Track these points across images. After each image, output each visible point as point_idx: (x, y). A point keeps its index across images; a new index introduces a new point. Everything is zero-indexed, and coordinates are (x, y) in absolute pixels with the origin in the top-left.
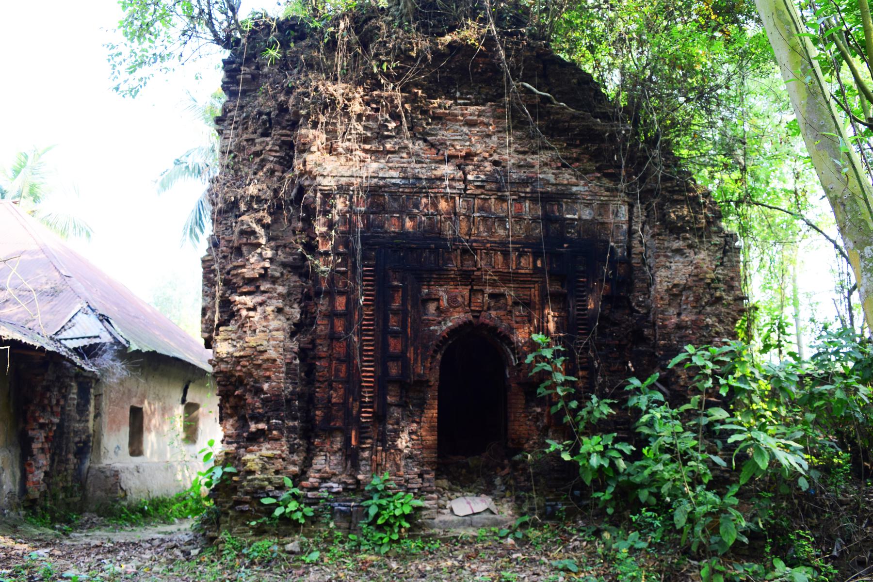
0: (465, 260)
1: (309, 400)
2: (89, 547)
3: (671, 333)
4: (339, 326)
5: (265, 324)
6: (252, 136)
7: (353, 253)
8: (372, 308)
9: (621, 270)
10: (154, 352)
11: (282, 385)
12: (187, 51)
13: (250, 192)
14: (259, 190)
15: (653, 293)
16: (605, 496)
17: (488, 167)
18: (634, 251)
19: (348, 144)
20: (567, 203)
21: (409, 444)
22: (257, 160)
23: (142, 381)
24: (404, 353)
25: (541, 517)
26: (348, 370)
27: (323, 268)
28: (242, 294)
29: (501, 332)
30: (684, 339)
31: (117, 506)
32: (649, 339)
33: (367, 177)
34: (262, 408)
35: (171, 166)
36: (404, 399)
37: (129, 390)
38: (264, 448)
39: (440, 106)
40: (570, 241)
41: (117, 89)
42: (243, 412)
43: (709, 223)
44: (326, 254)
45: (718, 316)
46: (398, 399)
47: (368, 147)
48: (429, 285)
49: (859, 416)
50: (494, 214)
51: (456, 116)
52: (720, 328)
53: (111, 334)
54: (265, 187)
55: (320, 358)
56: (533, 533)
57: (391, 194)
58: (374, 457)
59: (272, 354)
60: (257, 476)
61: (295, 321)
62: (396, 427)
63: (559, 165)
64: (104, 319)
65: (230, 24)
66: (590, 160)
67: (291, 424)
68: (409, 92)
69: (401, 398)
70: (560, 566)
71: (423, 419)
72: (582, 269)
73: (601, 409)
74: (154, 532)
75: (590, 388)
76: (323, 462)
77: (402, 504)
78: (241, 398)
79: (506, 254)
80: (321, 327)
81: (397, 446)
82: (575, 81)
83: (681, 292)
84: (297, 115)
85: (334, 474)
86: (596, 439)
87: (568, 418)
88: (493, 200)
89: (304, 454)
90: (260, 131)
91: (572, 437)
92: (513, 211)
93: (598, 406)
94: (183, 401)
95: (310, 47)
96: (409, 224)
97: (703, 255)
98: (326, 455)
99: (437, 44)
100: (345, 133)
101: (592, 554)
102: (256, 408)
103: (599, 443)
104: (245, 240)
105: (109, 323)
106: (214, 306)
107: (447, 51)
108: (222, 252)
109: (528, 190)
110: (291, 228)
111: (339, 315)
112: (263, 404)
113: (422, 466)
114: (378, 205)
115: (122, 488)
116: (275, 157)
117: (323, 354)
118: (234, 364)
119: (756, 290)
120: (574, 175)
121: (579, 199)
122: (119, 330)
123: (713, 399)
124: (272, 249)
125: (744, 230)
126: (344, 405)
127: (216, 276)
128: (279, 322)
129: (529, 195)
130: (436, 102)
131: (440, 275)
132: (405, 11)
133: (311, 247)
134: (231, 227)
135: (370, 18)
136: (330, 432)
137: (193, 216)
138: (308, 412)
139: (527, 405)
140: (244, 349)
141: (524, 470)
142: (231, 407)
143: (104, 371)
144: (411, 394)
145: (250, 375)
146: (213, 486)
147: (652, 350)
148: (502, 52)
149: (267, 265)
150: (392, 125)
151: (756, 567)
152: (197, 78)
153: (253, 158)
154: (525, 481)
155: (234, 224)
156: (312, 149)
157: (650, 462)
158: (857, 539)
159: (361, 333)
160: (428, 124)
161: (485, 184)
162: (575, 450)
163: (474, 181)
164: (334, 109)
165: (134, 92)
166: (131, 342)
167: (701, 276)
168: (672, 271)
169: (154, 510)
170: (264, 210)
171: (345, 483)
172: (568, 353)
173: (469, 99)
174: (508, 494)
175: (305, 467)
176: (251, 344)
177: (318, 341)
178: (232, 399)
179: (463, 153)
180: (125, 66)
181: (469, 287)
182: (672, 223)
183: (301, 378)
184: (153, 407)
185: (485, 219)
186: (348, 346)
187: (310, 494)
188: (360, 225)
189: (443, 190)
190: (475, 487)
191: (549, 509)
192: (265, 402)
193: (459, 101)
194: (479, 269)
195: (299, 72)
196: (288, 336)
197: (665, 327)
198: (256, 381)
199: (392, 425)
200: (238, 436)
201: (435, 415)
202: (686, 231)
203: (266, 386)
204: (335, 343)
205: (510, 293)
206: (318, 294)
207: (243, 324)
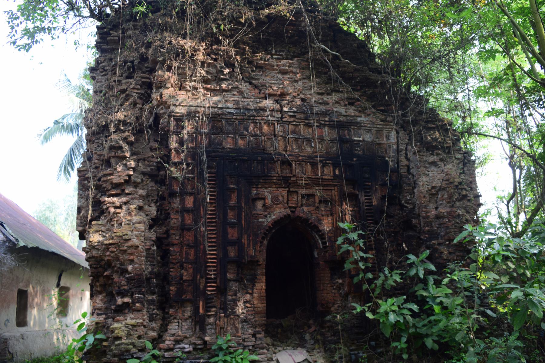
0: (283, 169)
3: (432, 222)
4: (189, 219)
5: (129, 218)
6: (120, 78)
8: (214, 205)
10: (37, 248)
13: (118, 117)
14: (125, 116)
16: (402, 344)
18: (401, 164)
19: (193, 83)
20: (354, 129)
21: (244, 311)
22: (123, 96)
23: (28, 270)
26: (196, 254)
28: (109, 196)
29: (311, 223)
30: (442, 226)
32: (416, 227)
33: (209, 107)
34: (127, 285)
35: (52, 125)
36: (240, 275)
37: (17, 277)
38: (129, 318)
39: (261, 59)
40: (358, 156)
42: (110, 289)
45: (465, 208)
46: (235, 275)
47: (209, 86)
50: (303, 136)
53: (4, 234)
54: (130, 114)
55: (173, 245)
57: (227, 120)
58: (218, 322)
59: (135, 241)
60: (123, 341)
61: (153, 216)
62: (234, 297)
63: (347, 103)
66: (367, 100)
67: (150, 297)
68: (239, 48)
69: (238, 274)
71: (255, 290)
72: (367, 176)
76: (177, 327)
77: (242, 359)
79: (314, 165)
80: (175, 220)
81: (235, 312)
82: (355, 45)
83: (437, 192)
85: (186, 337)
87: (365, 286)
88: (302, 126)
89: (161, 322)
90: (125, 75)
93: (391, 276)
94: (58, 285)
95: (165, 15)
96: (241, 142)
97: (450, 166)
98: (178, 322)
99: (259, 15)
100: (191, 76)
102: (122, 286)
103: (393, 304)
104: (113, 154)
105: (3, 226)
106: (88, 206)
107: (266, 20)
108: (95, 163)
109: (327, 119)
110: (149, 146)
111: (188, 211)
112: (128, 282)
113: (255, 328)
114: (217, 128)
115: (9, 352)
116: (137, 93)
121: (362, 126)
122: (10, 232)
124: (135, 161)
126: (193, 281)
127: (89, 182)
128: (140, 217)
129: (327, 123)
131: (265, 180)
133: (167, 158)
134: (102, 144)
136: (181, 303)
137: (66, 159)
140: (112, 238)
142: (100, 285)
144: (245, 269)
145: (117, 259)
146: (85, 350)
147: (418, 235)
149: (131, 173)
150: (227, 71)
152: (75, 44)
154: (332, 336)
155: (104, 142)
156: (169, 85)
159: (205, 224)
160: (253, 71)
161: (296, 114)
163: (288, 112)
165: (27, 47)
166: (19, 240)
167: (451, 180)
170: (129, 131)
171: (194, 344)
173: (281, 55)
174: (317, 346)
175: (162, 332)
177: (172, 232)
178: (101, 279)
179: (279, 93)
181: (287, 189)
182: (428, 143)
183: (158, 261)
184: (35, 290)
185: (296, 140)
187: (166, 354)
189: (266, 118)
190: (291, 342)
191: (353, 357)
192: (129, 280)
193: (274, 57)
194: (294, 176)
196: (147, 228)
197: (428, 217)
198: (122, 264)
200: (106, 308)
201: (264, 287)
202: (439, 149)
203: (130, 268)
204: (185, 232)
205: (318, 193)
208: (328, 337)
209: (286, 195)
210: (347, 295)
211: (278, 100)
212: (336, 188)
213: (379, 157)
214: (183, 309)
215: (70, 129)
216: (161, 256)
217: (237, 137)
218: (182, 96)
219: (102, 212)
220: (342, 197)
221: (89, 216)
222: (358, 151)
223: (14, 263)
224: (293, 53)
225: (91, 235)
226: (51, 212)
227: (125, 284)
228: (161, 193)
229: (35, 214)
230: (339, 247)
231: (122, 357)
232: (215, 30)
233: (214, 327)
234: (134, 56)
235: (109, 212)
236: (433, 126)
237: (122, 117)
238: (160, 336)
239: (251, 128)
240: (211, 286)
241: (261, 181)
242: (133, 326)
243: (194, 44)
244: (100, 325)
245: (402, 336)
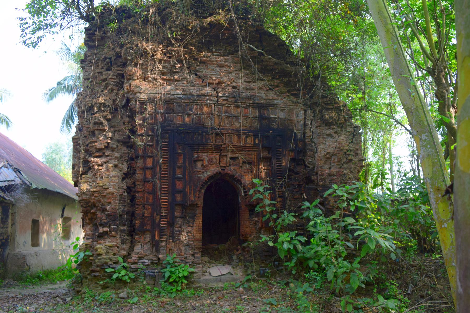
0: (217, 139)
2: (8, 298)
4: (149, 174)
5: (108, 173)
6: (101, 71)
7: (157, 136)
8: (167, 165)
9: (300, 145)
10: (46, 189)
12: (65, 23)
14: (105, 100)
15: (316, 157)
16: (292, 264)
17: (230, 89)
18: (307, 135)
19: (154, 75)
20: (271, 109)
22: (104, 83)
23: (39, 205)
24: (184, 189)
25: (257, 276)
27: (140, 143)
28: (94, 157)
29: (236, 178)
30: (332, 181)
31: (24, 275)
32: (314, 181)
33: (164, 94)
35: (55, 85)
38: (107, 242)
39: (204, 56)
40: (273, 129)
41: (25, 42)
42: (95, 222)
43: (345, 120)
44: (142, 135)
45: (350, 169)
47: (165, 77)
49: (422, 221)
52: (351, 176)
53: (21, 179)
54: (108, 99)
55: (138, 192)
56: (253, 285)
57: (178, 103)
58: (168, 245)
59: (112, 190)
60: (103, 257)
62: (179, 229)
63: (268, 89)
64: (17, 170)
65: (89, 8)
66: (284, 86)
67: (122, 228)
68: (188, 48)
69: (182, 213)
70: (268, 302)
71: (195, 224)
72: (279, 144)
73: (289, 218)
74: (46, 288)
75: (284, 208)
77: (183, 270)
78: (94, 214)
79: (239, 136)
80: (139, 175)
81: (180, 239)
82: (276, 44)
83: (331, 156)
84: (126, 59)
85: (146, 255)
86: (287, 234)
87: (271, 224)
88: (232, 107)
89: (130, 245)
90: (105, 68)
91: (274, 234)
92: (243, 113)
94: (62, 216)
95: (134, 22)
96: (187, 119)
97: (342, 137)
100: (152, 70)
101: (284, 295)
103: (288, 237)
107: (208, 26)
108: (84, 134)
109: (251, 102)
110: (122, 121)
112: (107, 217)
113: (194, 250)
114: (170, 109)
115: (27, 265)
116: (113, 82)
117: (140, 190)
119: (371, 156)
122: (26, 177)
123: (347, 213)
124: (112, 133)
125: (365, 124)
127: (80, 147)
128: (116, 173)
129: (252, 105)
131: (203, 147)
132: (186, 4)
133: (133, 132)
135: (167, 8)
138: (132, 221)
140: (96, 187)
141: (249, 251)
143: (17, 200)
144: (187, 209)
145: (100, 201)
146: (79, 263)
148: (238, 28)
149: (109, 141)
151: (369, 300)
152: (70, 38)
157: (314, 246)
158: (420, 284)
159: (160, 178)
160: (198, 66)
161: (228, 98)
162: (275, 241)
164: (146, 56)
165: (34, 45)
166: (32, 183)
167: (341, 148)
169: (45, 277)
170: (107, 111)
171: (152, 260)
172: (272, 189)
173: (220, 53)
174: (240, 264)
176: (100, 185)
178: (89, 215)
179: (217, 82)
180: (29, 30)
185: (228, 117)
186: (154, 185)
187: (133, 266)
188: (161, 120)
189: (206, 102)
191: (262, 272)
192: (108, 216)
193: (214, 54)
194: (224, 144)
195: (127, 36)
196: (121, 180)
197: (322, 175)
198: (103, 205)
200: (93, 235)
201: (201, 222)
202: (334, 125)
203: (108, 208)
204: (146, 184)
205: (241, 157)
206: (137, 157)
207: (95, 174)
208: (246, 258)
209: (219, 158)
210: (260, 229)
212: (255, 153)
214: (144, 236)
215: (70, 89)
216: (130, 200)
217: (185, 116)
218: (144, 86)
219: (90, 168)
220: (259, 159)
223: (29, 201)
226: (57, 155)
227: (105, 218)
228: (130, 155)
229: (44, 160)
230: (252, 196)
231: (102, 267)
232: (169, 36)
234: (111, 54)
235: (94, 169)
236: (332, 107)
237: (103, 101)
240: (163, 221)
241: (201, 148)
242: (110, 247)
243: (154, 46)
244: (88, 246)
245: (293, 258)
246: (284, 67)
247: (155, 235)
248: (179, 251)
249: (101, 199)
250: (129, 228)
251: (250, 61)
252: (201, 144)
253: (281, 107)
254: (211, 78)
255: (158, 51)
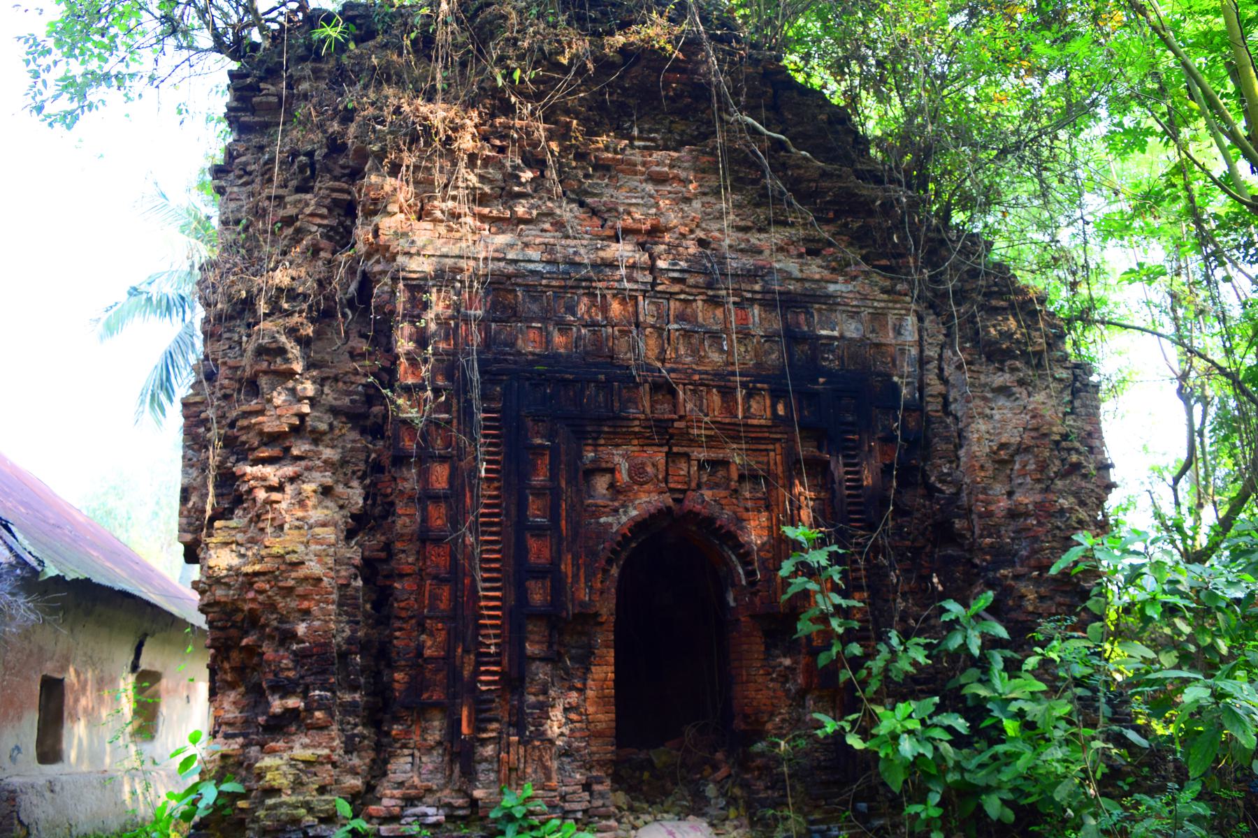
0: (656, 402)
1: (381, 654)
4: (438, 517)
5: (300, 514)
6: (281, 192)
7: (463, 387)
8: (496, 484)
10: (88, 580)
11: (332, 626)
13: (277, 281)
14: (293, 279)
15: (963, 459)
19: (450, 204)
20: (819, 310)
21: (566, 730)
22: (290, 231)
24: (555, 563)
26: (454, 597)
28: (255, 462)
29: (721, 527)
32: (963, 536)
33: (486, 259)
34: (294, 669)
35: (123, 297)
36: (555, 647)
37: (41, 649)
38: (297, 745)
39: (607, 149)
40: (829, 373)
42: (255, 677)
45: (1076, 494)
46: (545, 646)
47: (486, 211)
48: (596, 445)
50: (702, 326)
51: (635, 165)
53: (11, 549)
54: (303, 274)
55: (402, 576)
57: (528, 288)
58: (503, 755)
59: (314, 567)
60: (284, 798)
61: (355, 509)
62: (541, 698)
63: (803, 250)
66: (851, 244)
67: (348, 697)
68: (556, 123)
69: (550, 646)
71: (590, 682)
72: (850, 419)
79: (727, 393)
80: (405, 520)
81: (544, 733)
82: (823, 117)
83: (1012, 456)
85: (429, 790)
86: (903, 708)
87: (845, 675)
88: (700, 303)
89: (372, 754)
90: (294, 183)
93: (906, 650)
94: (135, 667)
95: (385, 46)
96: (558, 339)
97: (1040, 397)
98: (412, 755)
99: (603, 47)
102: (282, 670)
103: (910, 716)
104: (265, 365)
105: (9, 531)
106: (205, 485)
107: (618, 59)
108: (222, 387)
109: (757, 287)
111: (436, 498)
112: (296, 662)
113: (589, 769)
115: (21, 822)
116: (319, 226)
117: (407, 569)
118: (241, 589)
120: (827, 268)
121: (839, 304)
122: (26, 543)
124: (314, 382)
126: (448, 661)
127: (209, 430)
128: (326, 512)
129: (759, 296)
130: (603, 140)
131: (613, 425)
133: (388, 375)
134: (240, 343)
136: (419, 710)
138: (378, 674)
139: (768, 655)
142: (232, 668)
144: (567, 633)
145: (272, 607)
147: (968, 556)
149: (306, 409)
150: (527, 175)
153: (280, 229)
155: (245, 339)
156: (393, 208)
159: (474, 528)
160: (587, 176)
161: (686, 276)
165: (69, 119)
166: (46, 561)
167: (1044, 430)
168: (993, 423)
170: (301, 312)
171: (449, 805)
174: (732, 813)
175: (374, 777)
176: (275, 550)
178: (235, 656)
179: (647, 226)
181: (665, 449)
182: (991, 343)
183: (365, 613)
184: (82, 677)
185: (687, 334)
189: (616, 285)
190: (673, 803)
192: (300, 657)
194: (681, 418)
195: (366, 87)
196: (342, 536)
197: (990, 514)
198: (282, 620)
199: (534, 695)
200: (246, 722)
201: (611, 676)
202: (1015, 357)
203: (301, 629)
204: (429, 547)
205: (737, 457)
207: (259, 516)
210: (802, 694)
211: (646, 243)
212: (777, 445)
213: (879, 374)
215: (166, 307)
217: (551, 328)
218: (423, 232)
219: (238, 500)
220: (793, 467)
221: (208, 508)
222: (830, 361)
223: (33, 617)
224: (681, 135)
225: (212, 552)
227: (291, 665)
228: (373, 456)
230: (786, 583)
232: (500, 82)
233: (496, 766)
234: (314, 141)
235: (254, 500)
236: (1002, 303)
237: (287, 281)
238: (370, 788)
239: (582, 308)
241: (606, 429)
242: (308, 763)
244: (231, 761)
246: (851, 185)
247: (459, 721)
248: (541, 774)
249: (278, 598)
250: (371, 699)
251: (759, 157)
252: (609, 419)
253: (847, 305)
254: (629, 213)
255: (463, 127)
